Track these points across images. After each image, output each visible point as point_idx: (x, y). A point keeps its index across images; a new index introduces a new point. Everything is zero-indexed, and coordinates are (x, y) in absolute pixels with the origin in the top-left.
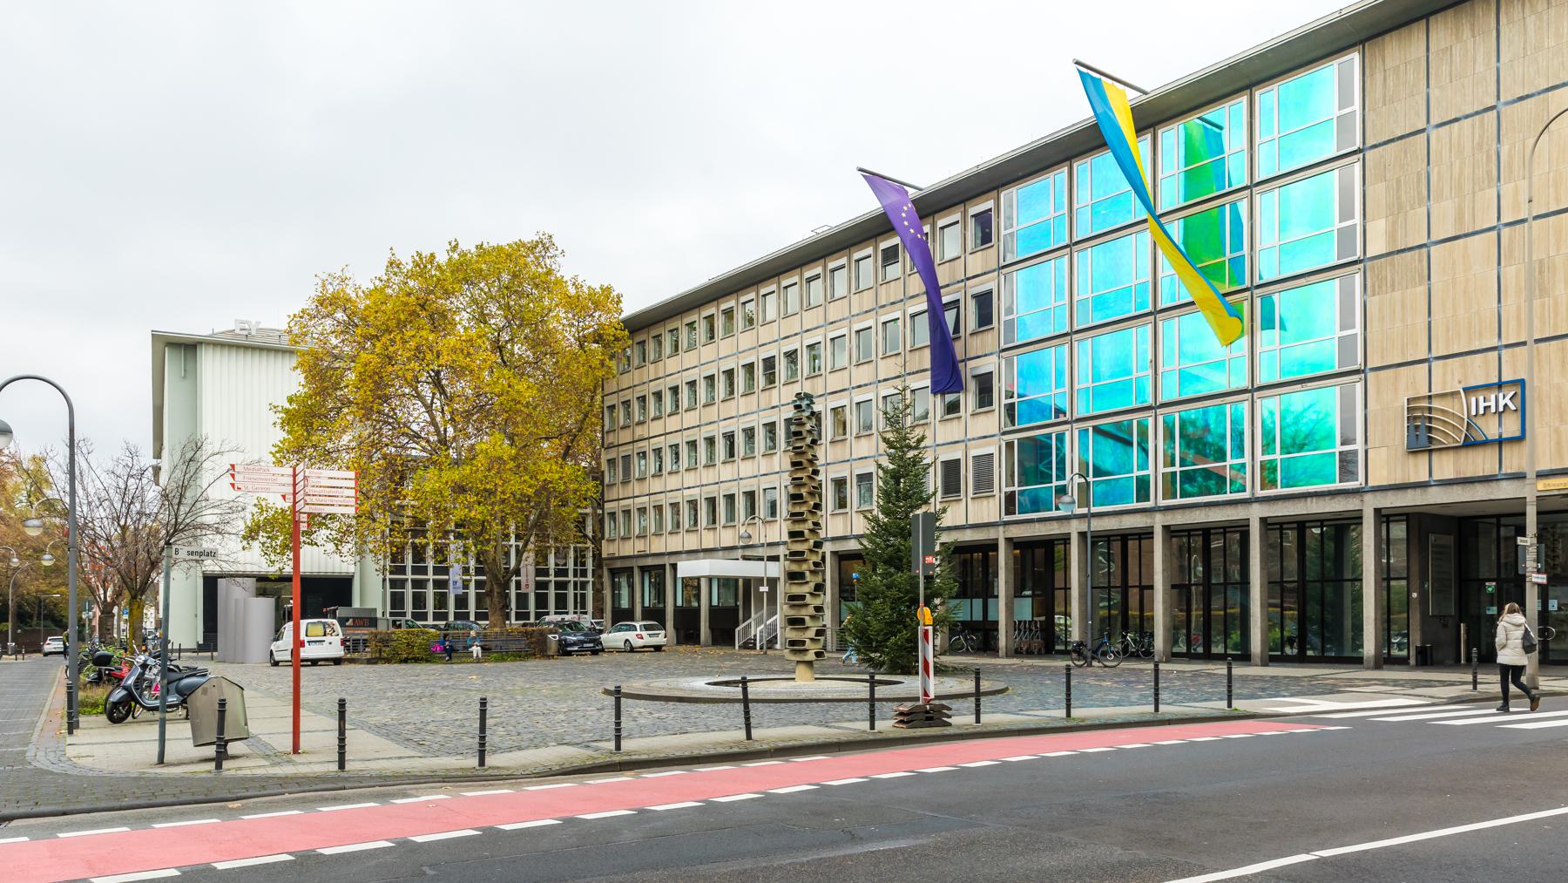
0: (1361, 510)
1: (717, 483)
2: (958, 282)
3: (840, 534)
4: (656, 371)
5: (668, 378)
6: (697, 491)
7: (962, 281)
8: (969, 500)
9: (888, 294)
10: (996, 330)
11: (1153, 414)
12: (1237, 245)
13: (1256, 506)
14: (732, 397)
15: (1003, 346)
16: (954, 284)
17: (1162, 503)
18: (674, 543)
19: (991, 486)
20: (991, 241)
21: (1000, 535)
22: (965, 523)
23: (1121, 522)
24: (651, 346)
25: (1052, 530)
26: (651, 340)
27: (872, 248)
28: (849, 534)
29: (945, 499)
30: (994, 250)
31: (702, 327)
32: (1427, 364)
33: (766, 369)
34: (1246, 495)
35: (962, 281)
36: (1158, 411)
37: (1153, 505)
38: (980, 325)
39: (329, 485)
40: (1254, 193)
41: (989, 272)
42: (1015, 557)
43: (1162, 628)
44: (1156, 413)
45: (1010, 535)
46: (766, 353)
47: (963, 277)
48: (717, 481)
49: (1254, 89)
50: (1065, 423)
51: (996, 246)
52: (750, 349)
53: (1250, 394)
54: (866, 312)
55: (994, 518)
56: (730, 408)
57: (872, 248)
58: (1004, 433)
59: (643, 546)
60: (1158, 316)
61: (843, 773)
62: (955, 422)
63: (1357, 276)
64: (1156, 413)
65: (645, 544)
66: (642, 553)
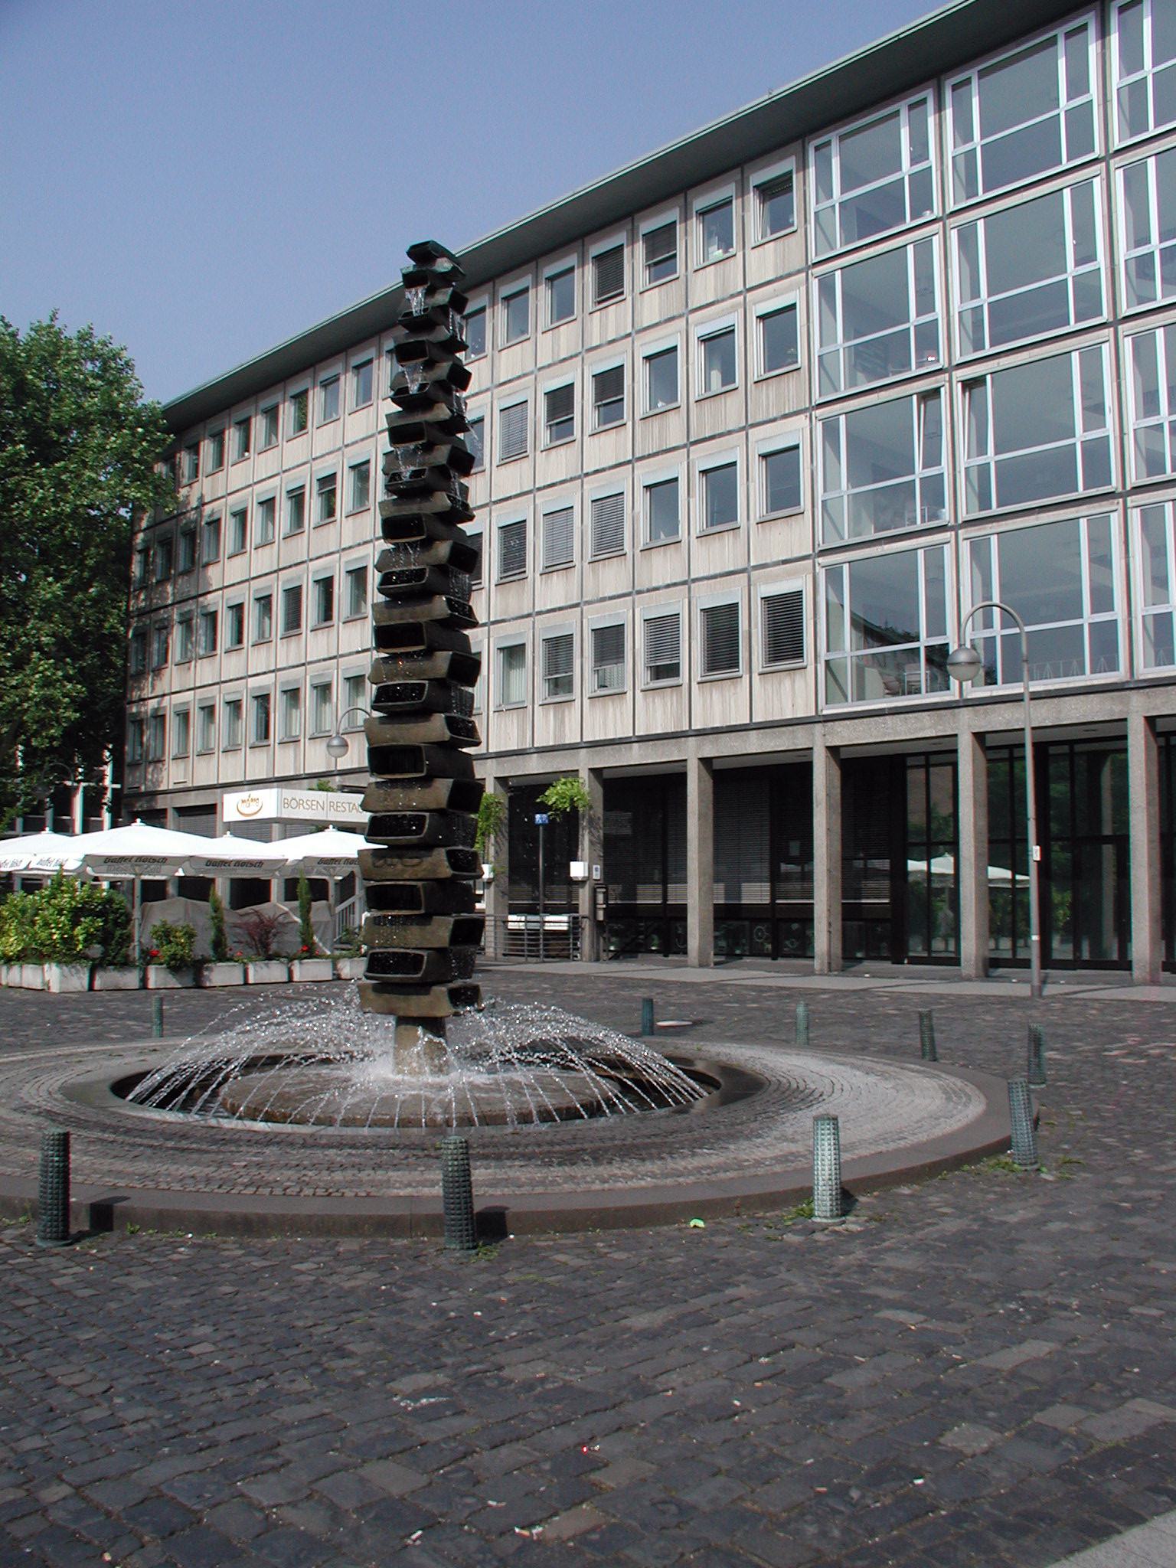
0: (956, 735)
1: (303, 665)
2: (732, 296)
3: (513, 746)
4: (603, 327)
5: (230, 498)
6: (188, 696)
7: (739, 293)
8: (755, 677)
9: (603, 327)
10: (805, 371)
11: (1120, 507)
12: (1086, 255)
13: (965, 714)
14: (332, 519)
15: (817, 399)
16: (723, 300)
17: (1146, 671)
18: (230, 769)
19: (798, 653)
20: (573, 313)
21: (818, 742)
22: (579, 740)
23: (1060, 712)
24: (259, 424)
25: (922, 729)
26: (752, 200)
27: (793, 158)
28: (528, 745)
29: (704, 679)
30: (799, 238)
31: (586, 278)
32: (746, 575)
33: (552, 413)
34: (1119, 676)
35: (739, 293)
36: (1129, 499)
37: (485, 751)
38: (769, 367)
39: (264, 483)
40: (1112, 169)
41: (789, 275)
42: (1159, 748)
43: (1147, 916)
44: (1125, 503)
45: (836, 742)
46: (323, 469)
47: (740, 288)
48: (303, 661)
49: (943, 77)
50: (943, 528)
51: (801, 232)
52: (363, 440)
53: (953, 533)
54: (565, 360)
55: (805, 710)
56: (298, 548)
57: (677, 210)
58: (823, 553)
59: (182, 773)
60: (1120, 327)
61: (824, 1221)
62: (728, 538)
63: (1105, 347)
64: (1125, 503)
65: (185, 770)
66: (181, 786)
